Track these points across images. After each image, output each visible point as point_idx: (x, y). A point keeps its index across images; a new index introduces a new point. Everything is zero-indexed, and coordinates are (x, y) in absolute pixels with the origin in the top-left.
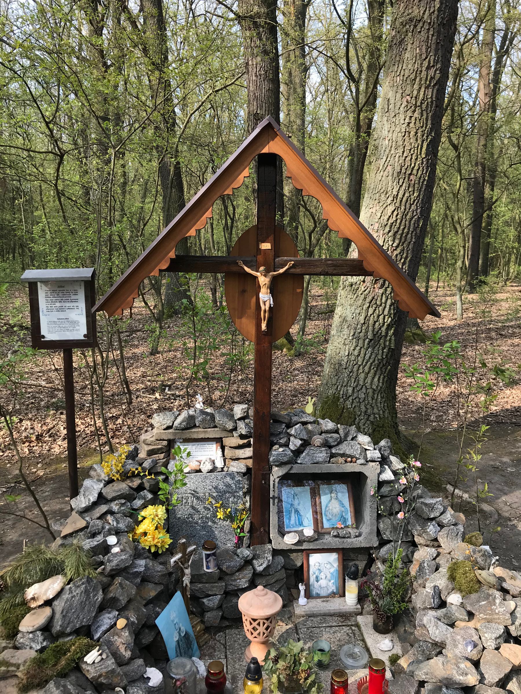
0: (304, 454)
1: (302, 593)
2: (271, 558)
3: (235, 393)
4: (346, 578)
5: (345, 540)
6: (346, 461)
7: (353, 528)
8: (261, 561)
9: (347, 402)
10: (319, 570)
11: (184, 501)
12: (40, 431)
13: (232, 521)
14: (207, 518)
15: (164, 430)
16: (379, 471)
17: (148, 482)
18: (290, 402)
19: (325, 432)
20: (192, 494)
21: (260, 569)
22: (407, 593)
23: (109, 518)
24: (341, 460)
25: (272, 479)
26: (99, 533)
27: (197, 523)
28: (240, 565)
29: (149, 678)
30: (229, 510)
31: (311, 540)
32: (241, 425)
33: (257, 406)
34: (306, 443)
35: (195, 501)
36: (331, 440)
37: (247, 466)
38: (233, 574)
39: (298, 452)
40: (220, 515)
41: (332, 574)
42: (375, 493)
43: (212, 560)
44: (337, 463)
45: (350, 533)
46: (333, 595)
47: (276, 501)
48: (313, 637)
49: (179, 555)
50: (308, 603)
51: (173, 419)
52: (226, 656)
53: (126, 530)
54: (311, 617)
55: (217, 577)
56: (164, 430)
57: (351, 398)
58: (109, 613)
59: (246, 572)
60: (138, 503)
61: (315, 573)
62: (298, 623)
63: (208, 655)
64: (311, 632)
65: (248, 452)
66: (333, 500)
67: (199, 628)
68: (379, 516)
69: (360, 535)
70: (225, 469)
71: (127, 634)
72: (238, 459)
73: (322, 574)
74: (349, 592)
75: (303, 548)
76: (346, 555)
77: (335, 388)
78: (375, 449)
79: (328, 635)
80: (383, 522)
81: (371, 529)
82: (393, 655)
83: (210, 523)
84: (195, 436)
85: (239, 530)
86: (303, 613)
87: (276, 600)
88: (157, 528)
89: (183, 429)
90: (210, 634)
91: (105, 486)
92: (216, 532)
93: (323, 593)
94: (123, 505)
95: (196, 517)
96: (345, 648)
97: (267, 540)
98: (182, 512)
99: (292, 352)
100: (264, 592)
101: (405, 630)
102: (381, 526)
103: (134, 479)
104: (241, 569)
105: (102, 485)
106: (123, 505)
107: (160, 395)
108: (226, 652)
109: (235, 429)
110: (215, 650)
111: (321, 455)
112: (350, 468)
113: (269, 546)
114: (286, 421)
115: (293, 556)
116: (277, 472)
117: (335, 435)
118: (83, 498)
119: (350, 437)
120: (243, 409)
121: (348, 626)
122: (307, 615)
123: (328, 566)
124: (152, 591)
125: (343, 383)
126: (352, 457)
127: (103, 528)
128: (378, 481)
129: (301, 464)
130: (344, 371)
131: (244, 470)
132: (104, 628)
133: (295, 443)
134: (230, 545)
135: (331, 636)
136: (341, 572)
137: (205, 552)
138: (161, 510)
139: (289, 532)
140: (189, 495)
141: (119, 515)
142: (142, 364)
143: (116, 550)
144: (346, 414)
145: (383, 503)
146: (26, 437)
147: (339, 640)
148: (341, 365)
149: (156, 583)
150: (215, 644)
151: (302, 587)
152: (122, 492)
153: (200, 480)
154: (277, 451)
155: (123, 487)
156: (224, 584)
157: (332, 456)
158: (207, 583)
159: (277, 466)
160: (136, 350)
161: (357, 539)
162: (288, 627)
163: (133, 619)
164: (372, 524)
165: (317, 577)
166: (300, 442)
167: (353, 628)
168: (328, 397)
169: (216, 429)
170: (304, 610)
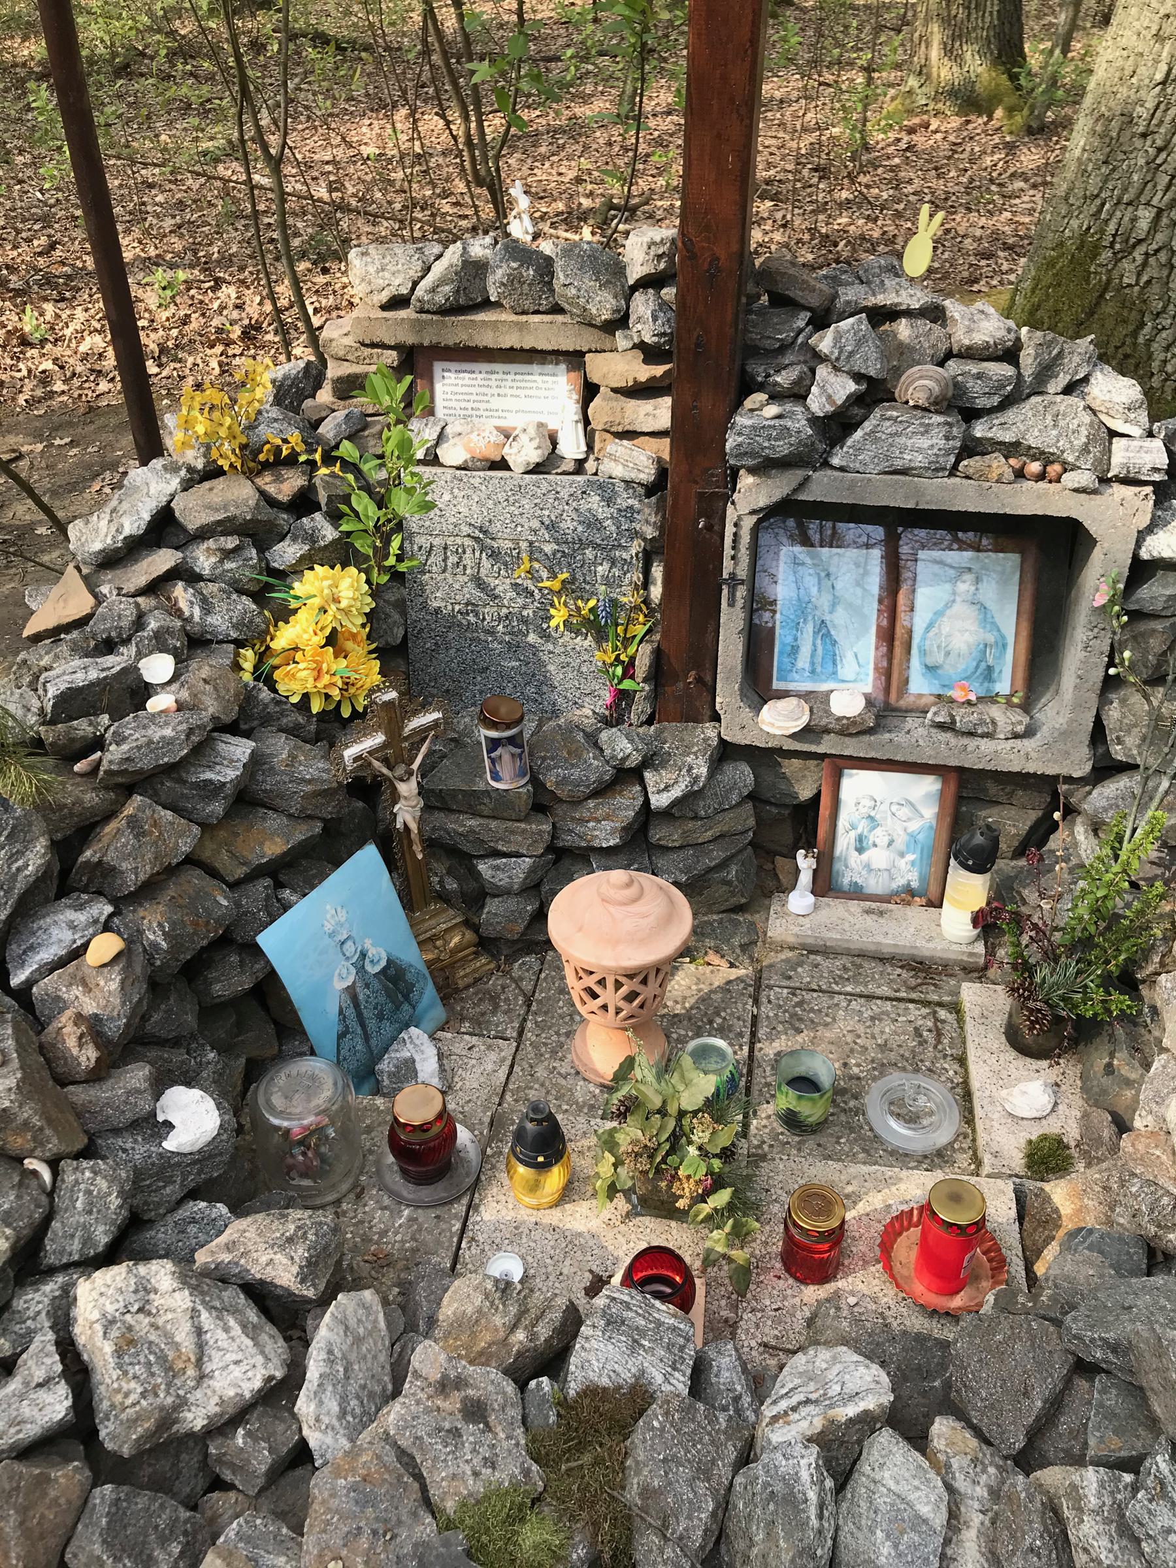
0: (859, 434)
1: (805, 878)
2: (704, 770)
3: (807, 237)
4: (952, 861)
5: (971, 743)
6: (1020, 474)
7: (1009, 703)
8: (667, 776)
9: (1125, 264)
10: (871, 818)
11: (453, 559)
12: (256, 316)
13: (601, 636)
14: (524, 621)
15: (384, 307)
16: (1144, 520)
17: (314, 487)
18: (966, 274)
19: (960, 356)
20: (476, 539)
21: (660, 801)
22: (1147, 959)
23: (181, 593)
24: (998, 464)
25: (731, 514)
26: (126, 642)
27: (491, 632)
28: (599, 781)
29: (169, 1126)
30: (592, 603)
31: (849, 729)
32: (643, 305)
33: (691, 230)
34: (874, 393)
35: (486, 563)
36: (976, 388)
37: (659, 460)
38: (578, 802)
39: (838, 426)
40: (558, 616)
41: (913, 837)
42: (1112, 601)
43: (506, 758)
44: (982, 477)
45: (994, 722)
46: (907, 895)
47: (741, 592)
48: (801, 1020)
49: (379, 739)
50: (816, 907)
51: (414, 273)
52: (521, 1033)
53: (234, 634)
54: (810, 952)
55: (524, 804)
56: (384, 307)
57: (1142, 249)
58: (80, 907)
59: (619, 800)
60: (287, 552)
61: (853, 827)
62: (771, 966)
63: (471, 1020)
64: (800, 1004)
65: (658, 413)
66: (959, 608)
67: (456, 940)
68: (1110, 684)
69: (1029, 733)
70: (590, 466)
71: (114, 985)
72: (630, 435)
73: (878, 831)
74: (955, 902)
75: (820, 749)
76: (969, 792)
77: (1093, 209)
78: (1150, 434)
79: (852, 1024)
80: (1123, 702)
81: (1072, 721)
82: (1044, 1138)
83: (532, 638)
84: (487, 339)
85: (619, 671)
86: (791, 940)
87: (669, 918)
88: (332, 640)
89: (444, 311)
90: (495, 957)
91: (187, 486)
92: (551, 668)
93: (874, 885)
94: (227, 554)
95: (489, 612)
96: (895, 1079)
97: (707, 713)
98: (445, 591)
99: (1019, 119)
100: (633, 891)
101: (1109, 1065)
102: (1113, 714)
103: (287, 473)
104: (603, 790)
105: (175, 483)
106: (227, 554)
107: (593, 233)
108: (525, 1020)
109: (621, 321)
110: (496, 1007)
111: (924, 442)
112: (1031, 499)
113: (710, 731)
114: (814, 301)
115: (791, 767)
116: (752, 494)
117: (1004, 370)
118: (103, 523)
119: (1062, 380)
120: (652, 244)
121: (926, 1003)
122: (803, 947)
123: (904, 812)
124: (272, 840)
125: (1125, 190)
126: (1048, 459)
127: (139, 622)
128: (1136, 557)
129: (842, 469)
130: (1138, 143)
131: (647, 474)
132: (46, 955)
133: (832, 389)
134: (586, 713)
135: (861, 1029)
136: (945, 836)
137: (486, 733)
138: (350, 586)
139: (783, 695)
140: (468, 542)
141: (211, 588)
142: (586, 147)
143: (159, 703)
144: (1109, 309)
145: (1137, 640)
146: (219, 331)
147: (883, 1047)
148: (1129, 119)
149: (290, 816)
150: (503, 988)
151: (805, 863)
152: (232, 511)
153: (501, 496)
154: (758, 415)
155: (236, 495)
156: (547, 827)
157: (971, 448)
158: (494, 818)
159: (752, 471)
160: (578, 110)
161: (1018, 743)
162: (734, 973)
163: (154, 936)
164: (1077, 706)
165: (860, 839)
166: (852, 386)
167: (942, 1014)
168: (1061, 244)
169: (560, 318)
170: (796, 930)
